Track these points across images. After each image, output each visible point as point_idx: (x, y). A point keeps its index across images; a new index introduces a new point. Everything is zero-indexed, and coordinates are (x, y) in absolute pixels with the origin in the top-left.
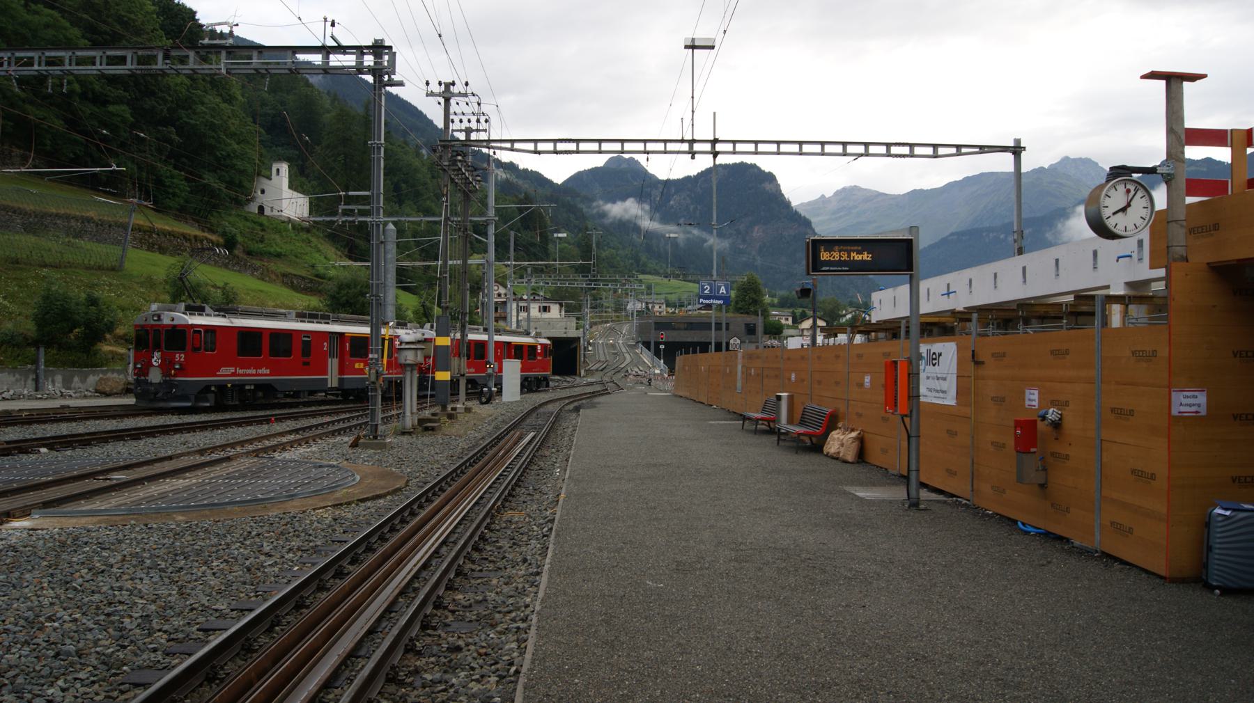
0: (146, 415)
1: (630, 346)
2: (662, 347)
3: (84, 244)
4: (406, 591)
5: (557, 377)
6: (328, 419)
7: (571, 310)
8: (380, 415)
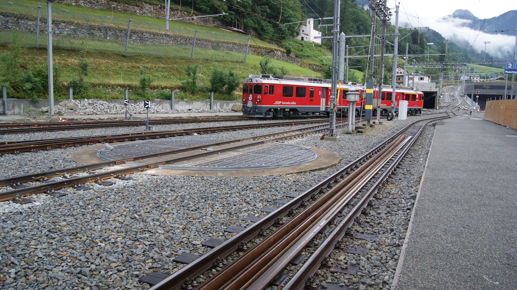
0: (245, 120)
1: (461, 96)
2: (477, 97)
3: (233, 53)
4: (310, 246)
5: (425, 109)
6: (318, 125)
7: (434, 79)
8: (334, 125)
